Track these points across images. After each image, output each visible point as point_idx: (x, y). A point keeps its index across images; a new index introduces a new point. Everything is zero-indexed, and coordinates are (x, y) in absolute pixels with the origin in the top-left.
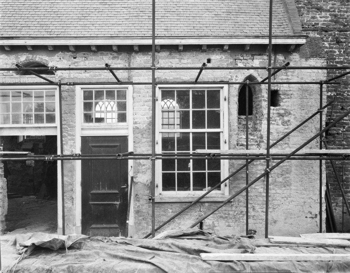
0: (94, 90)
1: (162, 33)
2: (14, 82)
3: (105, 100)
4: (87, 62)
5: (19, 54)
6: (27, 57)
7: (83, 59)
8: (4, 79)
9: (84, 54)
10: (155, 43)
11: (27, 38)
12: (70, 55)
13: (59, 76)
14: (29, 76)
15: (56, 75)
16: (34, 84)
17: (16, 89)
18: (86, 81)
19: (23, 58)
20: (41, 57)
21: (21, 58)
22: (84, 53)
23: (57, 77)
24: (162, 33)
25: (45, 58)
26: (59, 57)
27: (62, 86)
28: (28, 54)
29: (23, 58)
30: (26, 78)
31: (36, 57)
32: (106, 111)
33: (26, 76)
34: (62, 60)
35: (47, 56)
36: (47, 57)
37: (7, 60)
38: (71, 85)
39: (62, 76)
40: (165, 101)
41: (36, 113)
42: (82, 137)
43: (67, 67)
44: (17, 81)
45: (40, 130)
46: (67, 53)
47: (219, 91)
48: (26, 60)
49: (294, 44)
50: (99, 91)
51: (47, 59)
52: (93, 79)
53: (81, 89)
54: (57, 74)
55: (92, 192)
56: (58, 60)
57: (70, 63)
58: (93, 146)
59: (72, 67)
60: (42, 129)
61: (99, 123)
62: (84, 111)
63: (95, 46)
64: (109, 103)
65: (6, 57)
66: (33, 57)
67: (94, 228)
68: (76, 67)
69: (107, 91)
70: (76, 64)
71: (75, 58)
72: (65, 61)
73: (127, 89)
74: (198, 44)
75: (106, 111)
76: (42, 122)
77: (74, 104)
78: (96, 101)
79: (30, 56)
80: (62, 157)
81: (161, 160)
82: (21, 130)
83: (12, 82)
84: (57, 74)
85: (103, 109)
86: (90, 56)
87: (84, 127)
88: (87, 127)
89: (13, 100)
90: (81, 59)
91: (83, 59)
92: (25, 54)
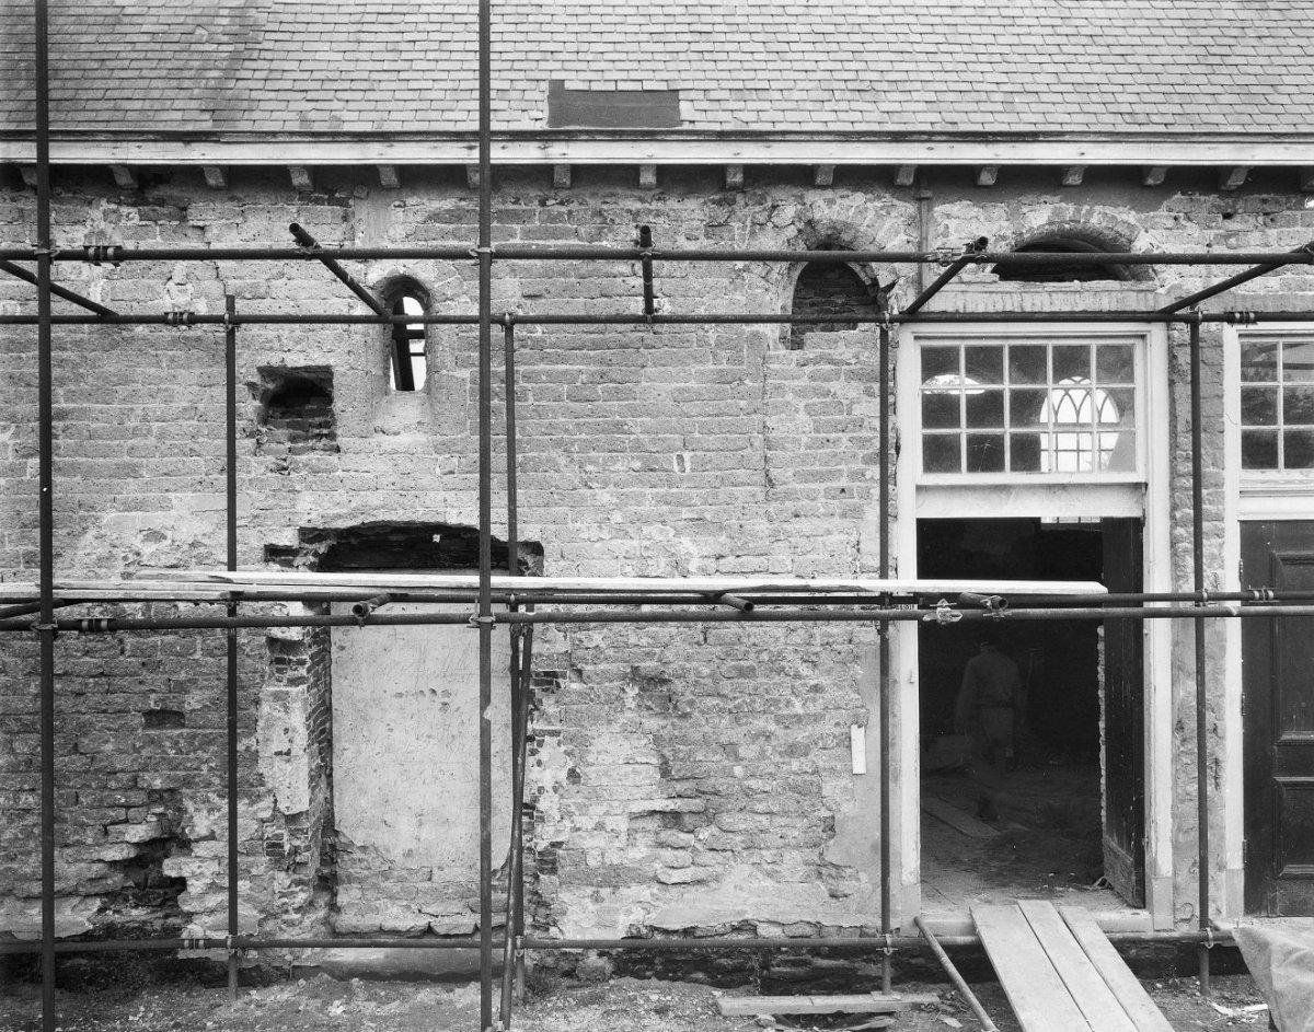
0: (1094, 344)
1: (921, 117)
2: (999, 308)
3: (1092, 382)
4: (1273, 232)
5: (1024, 199)
6: (1056, 212)
7: (1261, 219)
8: (960, 296)
9: (1264, 201)
10: (48, 159)
11: (1092, 138)
12: (1214, 206)
13: (1172, 287)
14: (1056, 284)
15: (1156, 282)
16: (1107, 316)
17: (986, 338)
18: (1271, 308)
19: (1040, 216)
20: (1109, 210)
21: (1030, 215)
22: (1265, 196)
23: (1161, 291)
24: (921, 117)
25: (1125, 217)
26: (1174, 214)
27: (516, 328)
28: (1057, 198)
29: (1040, 216)
30: (1046, 295)
31: (1090, 213)
32: (1056, 424)
33: (1045, 284)
34: (1184, 223)
35: (1133, 208)
36: (1133, 213)
37: (975, 224)
38: (182, 322)
39: (1180, 287)
40: (1066, 382)
41: (1272, 427)
42: (1242, 522)
43: (1201, 250)
44: (1011, 304)
45: (1064, 495)
46: (1203, 198)
47: (1130, 349)
48: (1051, 223)
49: (1161, 166)
50: (982, 349)
51: (1132, 221)
52: (1296, 297)
53: (916, 338)
54: (1165, 280)
55: (1285, 737)
56: (1170, 223)
57: (1210, 234)
58: (1285, 560)
59: (1218, 250)
60: (1075, 494)
61: (1304, 470)
62: (1243, 423)
63: (306, 167)
64: (1067, 394)
65: (975, 211)
66: (1079, 211)
67: (1295, 878)
68: (1232, 252)
69: (1013, 349)
70: (1233, 241)
71: (1227, 216)
72: (1192, 229)
73: (1138, 343)
74: (1112, 162)
75: (1056, 424)
76: (953, 466)
77: (1220, 397)
78: (1289, 384)
79: (1069, 210)
80: (1198, 599)
81: (915, 623)
82: (995, 497)
83: (991, 309)
84: (1165, 280)
85: (1085, 417)
86: (1289, 209)
87: (1249, 487)
88: (1260, 487)
89: (1287, 378)
90: (1252, 220)
91: (1261, 219)
92: (1048, 198)
